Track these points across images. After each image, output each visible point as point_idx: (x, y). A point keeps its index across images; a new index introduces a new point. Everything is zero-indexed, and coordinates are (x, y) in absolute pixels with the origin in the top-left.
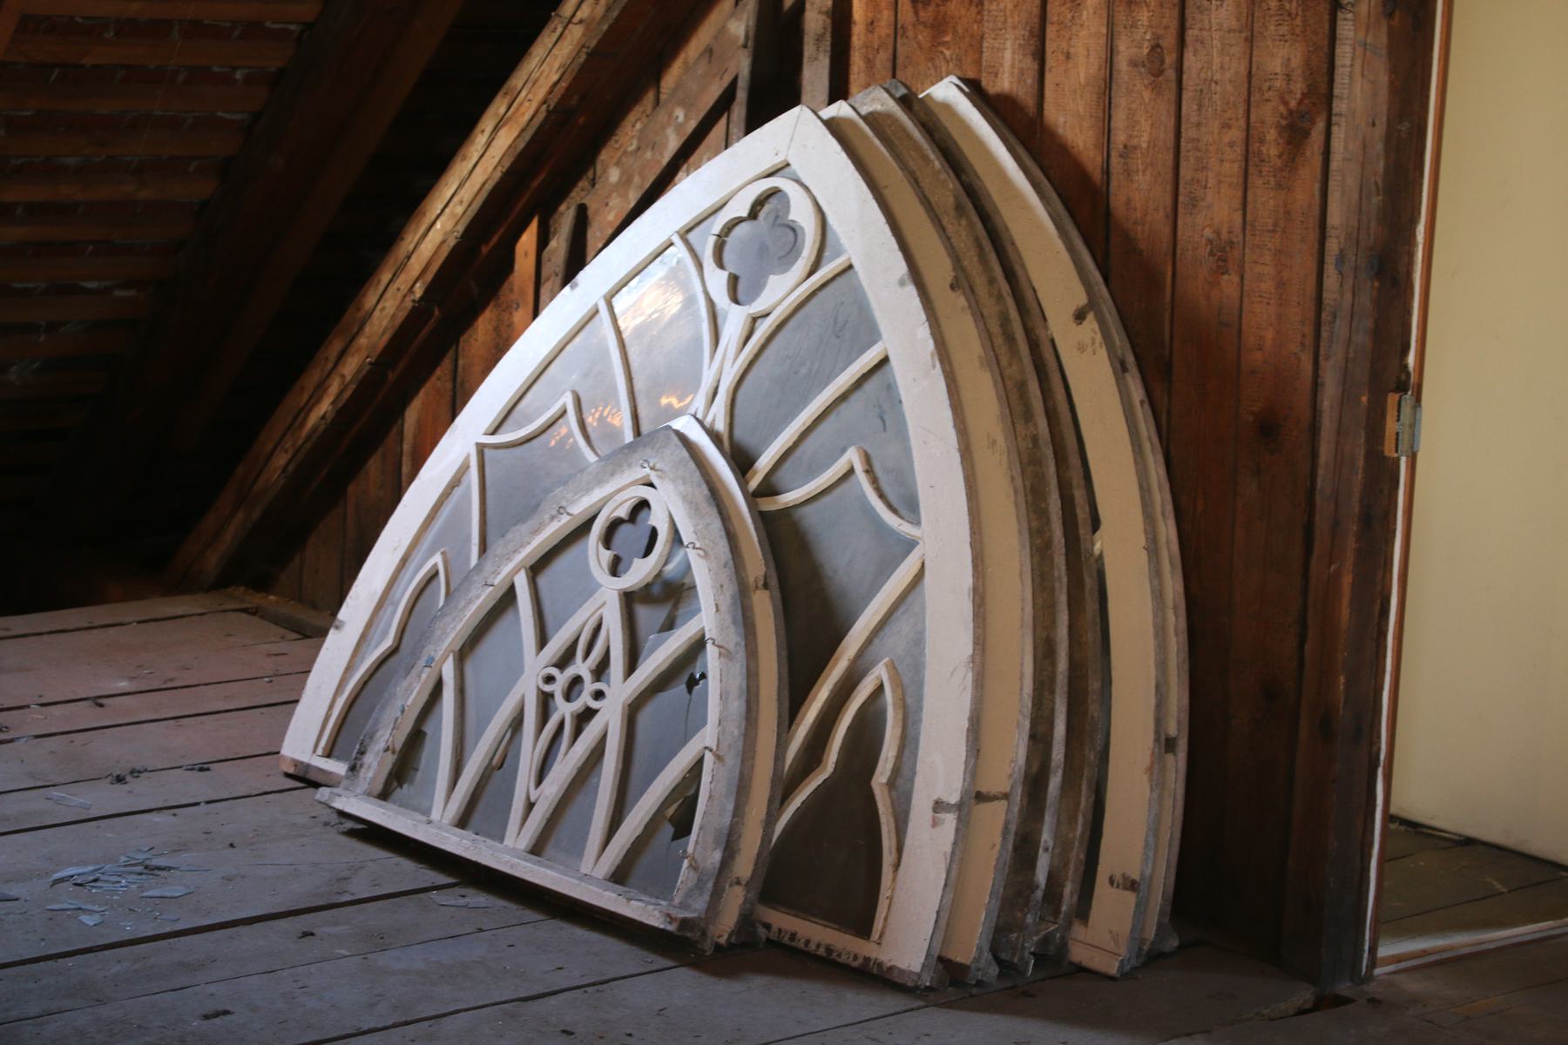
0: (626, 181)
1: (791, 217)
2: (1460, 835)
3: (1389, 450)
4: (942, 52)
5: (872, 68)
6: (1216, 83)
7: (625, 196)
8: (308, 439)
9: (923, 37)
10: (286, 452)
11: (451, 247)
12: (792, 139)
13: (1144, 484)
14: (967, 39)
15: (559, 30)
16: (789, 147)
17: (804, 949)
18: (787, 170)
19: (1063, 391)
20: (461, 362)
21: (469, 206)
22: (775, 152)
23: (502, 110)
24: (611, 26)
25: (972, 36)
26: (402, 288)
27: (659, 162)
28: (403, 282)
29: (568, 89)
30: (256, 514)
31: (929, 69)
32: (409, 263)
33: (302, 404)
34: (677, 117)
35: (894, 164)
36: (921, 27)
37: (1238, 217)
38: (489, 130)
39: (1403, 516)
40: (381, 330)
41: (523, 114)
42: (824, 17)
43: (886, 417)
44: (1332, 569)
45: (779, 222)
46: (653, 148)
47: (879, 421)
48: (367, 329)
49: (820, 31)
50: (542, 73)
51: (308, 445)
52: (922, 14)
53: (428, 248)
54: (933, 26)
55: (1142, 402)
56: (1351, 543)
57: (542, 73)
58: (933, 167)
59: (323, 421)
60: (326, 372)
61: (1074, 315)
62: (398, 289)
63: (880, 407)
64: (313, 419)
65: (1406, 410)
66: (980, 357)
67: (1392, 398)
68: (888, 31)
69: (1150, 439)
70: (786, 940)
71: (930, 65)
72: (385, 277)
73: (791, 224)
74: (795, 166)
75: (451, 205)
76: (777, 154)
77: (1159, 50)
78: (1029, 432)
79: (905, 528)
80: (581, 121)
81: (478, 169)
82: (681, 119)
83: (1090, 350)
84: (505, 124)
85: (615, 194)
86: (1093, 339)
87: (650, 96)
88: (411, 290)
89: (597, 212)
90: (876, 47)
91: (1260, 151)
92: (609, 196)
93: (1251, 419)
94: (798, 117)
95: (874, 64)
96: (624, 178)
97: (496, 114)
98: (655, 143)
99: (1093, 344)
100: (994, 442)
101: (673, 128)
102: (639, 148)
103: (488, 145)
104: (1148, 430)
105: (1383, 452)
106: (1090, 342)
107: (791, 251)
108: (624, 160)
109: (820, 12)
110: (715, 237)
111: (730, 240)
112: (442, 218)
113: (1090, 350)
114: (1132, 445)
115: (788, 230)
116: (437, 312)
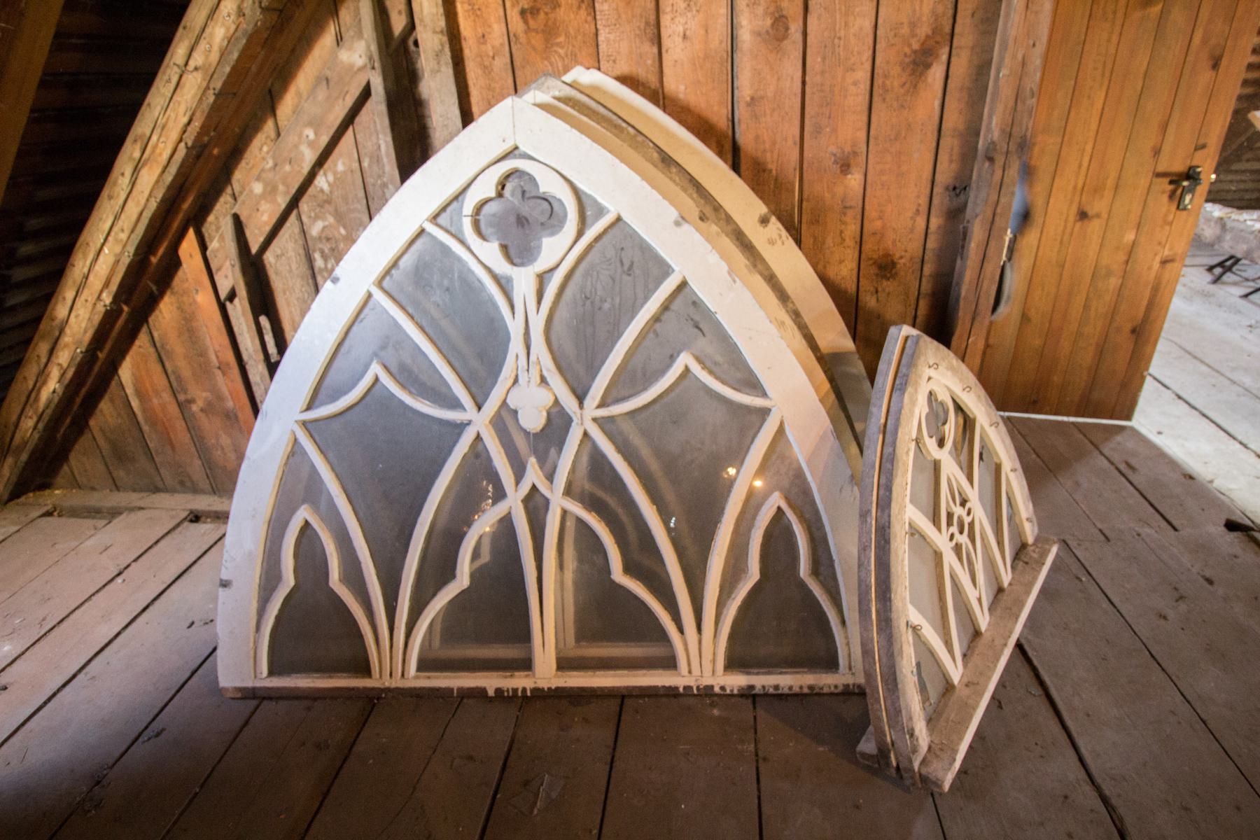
0: (271, 191)
1: (542, 190)
4: (556, 51)
5: (490, 73)
6: (840, 38)
7: (274, 201)
8: (47, 407)
9: (537, 40)
10: (31, 418)
11: (126, 266)
12: (514, 127)
14: (579, 38)
15: (175, 79)
16: (514, 134)
17: (790, 692)
18: (516, 152)
20: (156, 334)
21: (132, 231)
22: (502, 140)
23: (137, 154)
24: (234, 69)
25: (584, 34)
26: (89, 299)
27: (300, 172)
28: (88, 295)
29: (202, 128)
30: (24, 457)
31: (546, 66)
32: (88, 281)
33: (30, 387)
34: (307, 136)
35: (608, 134)
36: (534, 34)
37: (862, 135)
38: (128, 172)
40: (82, 331)
41: (160, 154)
42: (440, 36)
43: (701, 326)
45: (527, 195)
46: (290, 163)
47: (696, 330)
48: (68, 331)
49: (437, 47)
50: (168, 119)
51: (49, 411)
52: (531, 22)
53: (103, 267)
54: (543, 31)
57: (168, 119)
58: (628, 133)
59: (55, 395)
60: (42, 366)
62: (86, 301)
63: (692, 319)
64: (45, 394)
68: (501, 40)
70: (771, 690)
71: (546, 62)
72: (69, 294)
73: (543, 196)
74: (523, 148)
75: (113, 234)
76: (504, 141)
77: (784, 20)
79: (757, 402)
80: (216, 151)
81: (130, 204)
82: (312, 136)
83: (779, 242)
84: (142, 166)
85: (263, 202)
87: (269, 126)
88: (99, 298)
89: (250, 216)
90: (491, 54)
91: (884, 84)
92: (258, 203)
94: (513, 107)
95: (492, 70)
96: (269, 189)
97: (131, 158)
98: (291, 159)
101: (306, 145)
102: (276, 165)
103: (133, 184)
106: (778, 238)
107: (551, 215)
108: (264, 175)
109: (435, 32)
110: (469, 218)
111: (481, 217)
112: (108, 244)
115: (540, 201)
116: (126, 308)
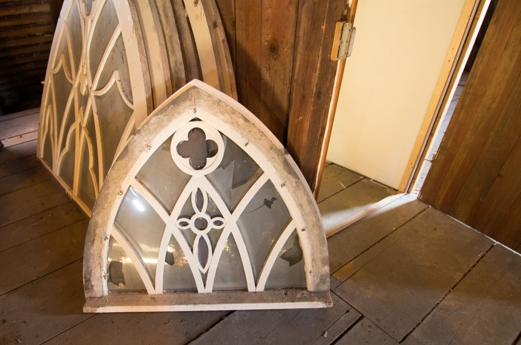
2: (330, 162)
3: (333, 57)
13: (222, 78)
19: (190, 38)
39: (336, 89)
44: (300, 118)
55: (223, 41)
56: (311, 108)
61: (194, 2)
65: (346, 32)
66: (153, 26)
67: (339, 25)
69: (226, 57)
78: (174, 59)
86: (201, 13)
93: (266, 44)
99: (201, 15)
100: (159, 65)
104: (225, 53)
105: (330, 58)
113: (200, 18)
114: (216, 61)
